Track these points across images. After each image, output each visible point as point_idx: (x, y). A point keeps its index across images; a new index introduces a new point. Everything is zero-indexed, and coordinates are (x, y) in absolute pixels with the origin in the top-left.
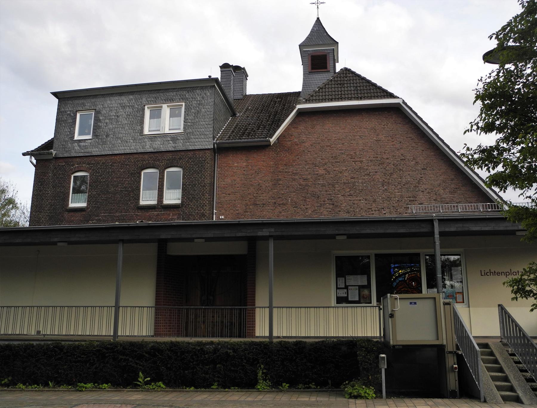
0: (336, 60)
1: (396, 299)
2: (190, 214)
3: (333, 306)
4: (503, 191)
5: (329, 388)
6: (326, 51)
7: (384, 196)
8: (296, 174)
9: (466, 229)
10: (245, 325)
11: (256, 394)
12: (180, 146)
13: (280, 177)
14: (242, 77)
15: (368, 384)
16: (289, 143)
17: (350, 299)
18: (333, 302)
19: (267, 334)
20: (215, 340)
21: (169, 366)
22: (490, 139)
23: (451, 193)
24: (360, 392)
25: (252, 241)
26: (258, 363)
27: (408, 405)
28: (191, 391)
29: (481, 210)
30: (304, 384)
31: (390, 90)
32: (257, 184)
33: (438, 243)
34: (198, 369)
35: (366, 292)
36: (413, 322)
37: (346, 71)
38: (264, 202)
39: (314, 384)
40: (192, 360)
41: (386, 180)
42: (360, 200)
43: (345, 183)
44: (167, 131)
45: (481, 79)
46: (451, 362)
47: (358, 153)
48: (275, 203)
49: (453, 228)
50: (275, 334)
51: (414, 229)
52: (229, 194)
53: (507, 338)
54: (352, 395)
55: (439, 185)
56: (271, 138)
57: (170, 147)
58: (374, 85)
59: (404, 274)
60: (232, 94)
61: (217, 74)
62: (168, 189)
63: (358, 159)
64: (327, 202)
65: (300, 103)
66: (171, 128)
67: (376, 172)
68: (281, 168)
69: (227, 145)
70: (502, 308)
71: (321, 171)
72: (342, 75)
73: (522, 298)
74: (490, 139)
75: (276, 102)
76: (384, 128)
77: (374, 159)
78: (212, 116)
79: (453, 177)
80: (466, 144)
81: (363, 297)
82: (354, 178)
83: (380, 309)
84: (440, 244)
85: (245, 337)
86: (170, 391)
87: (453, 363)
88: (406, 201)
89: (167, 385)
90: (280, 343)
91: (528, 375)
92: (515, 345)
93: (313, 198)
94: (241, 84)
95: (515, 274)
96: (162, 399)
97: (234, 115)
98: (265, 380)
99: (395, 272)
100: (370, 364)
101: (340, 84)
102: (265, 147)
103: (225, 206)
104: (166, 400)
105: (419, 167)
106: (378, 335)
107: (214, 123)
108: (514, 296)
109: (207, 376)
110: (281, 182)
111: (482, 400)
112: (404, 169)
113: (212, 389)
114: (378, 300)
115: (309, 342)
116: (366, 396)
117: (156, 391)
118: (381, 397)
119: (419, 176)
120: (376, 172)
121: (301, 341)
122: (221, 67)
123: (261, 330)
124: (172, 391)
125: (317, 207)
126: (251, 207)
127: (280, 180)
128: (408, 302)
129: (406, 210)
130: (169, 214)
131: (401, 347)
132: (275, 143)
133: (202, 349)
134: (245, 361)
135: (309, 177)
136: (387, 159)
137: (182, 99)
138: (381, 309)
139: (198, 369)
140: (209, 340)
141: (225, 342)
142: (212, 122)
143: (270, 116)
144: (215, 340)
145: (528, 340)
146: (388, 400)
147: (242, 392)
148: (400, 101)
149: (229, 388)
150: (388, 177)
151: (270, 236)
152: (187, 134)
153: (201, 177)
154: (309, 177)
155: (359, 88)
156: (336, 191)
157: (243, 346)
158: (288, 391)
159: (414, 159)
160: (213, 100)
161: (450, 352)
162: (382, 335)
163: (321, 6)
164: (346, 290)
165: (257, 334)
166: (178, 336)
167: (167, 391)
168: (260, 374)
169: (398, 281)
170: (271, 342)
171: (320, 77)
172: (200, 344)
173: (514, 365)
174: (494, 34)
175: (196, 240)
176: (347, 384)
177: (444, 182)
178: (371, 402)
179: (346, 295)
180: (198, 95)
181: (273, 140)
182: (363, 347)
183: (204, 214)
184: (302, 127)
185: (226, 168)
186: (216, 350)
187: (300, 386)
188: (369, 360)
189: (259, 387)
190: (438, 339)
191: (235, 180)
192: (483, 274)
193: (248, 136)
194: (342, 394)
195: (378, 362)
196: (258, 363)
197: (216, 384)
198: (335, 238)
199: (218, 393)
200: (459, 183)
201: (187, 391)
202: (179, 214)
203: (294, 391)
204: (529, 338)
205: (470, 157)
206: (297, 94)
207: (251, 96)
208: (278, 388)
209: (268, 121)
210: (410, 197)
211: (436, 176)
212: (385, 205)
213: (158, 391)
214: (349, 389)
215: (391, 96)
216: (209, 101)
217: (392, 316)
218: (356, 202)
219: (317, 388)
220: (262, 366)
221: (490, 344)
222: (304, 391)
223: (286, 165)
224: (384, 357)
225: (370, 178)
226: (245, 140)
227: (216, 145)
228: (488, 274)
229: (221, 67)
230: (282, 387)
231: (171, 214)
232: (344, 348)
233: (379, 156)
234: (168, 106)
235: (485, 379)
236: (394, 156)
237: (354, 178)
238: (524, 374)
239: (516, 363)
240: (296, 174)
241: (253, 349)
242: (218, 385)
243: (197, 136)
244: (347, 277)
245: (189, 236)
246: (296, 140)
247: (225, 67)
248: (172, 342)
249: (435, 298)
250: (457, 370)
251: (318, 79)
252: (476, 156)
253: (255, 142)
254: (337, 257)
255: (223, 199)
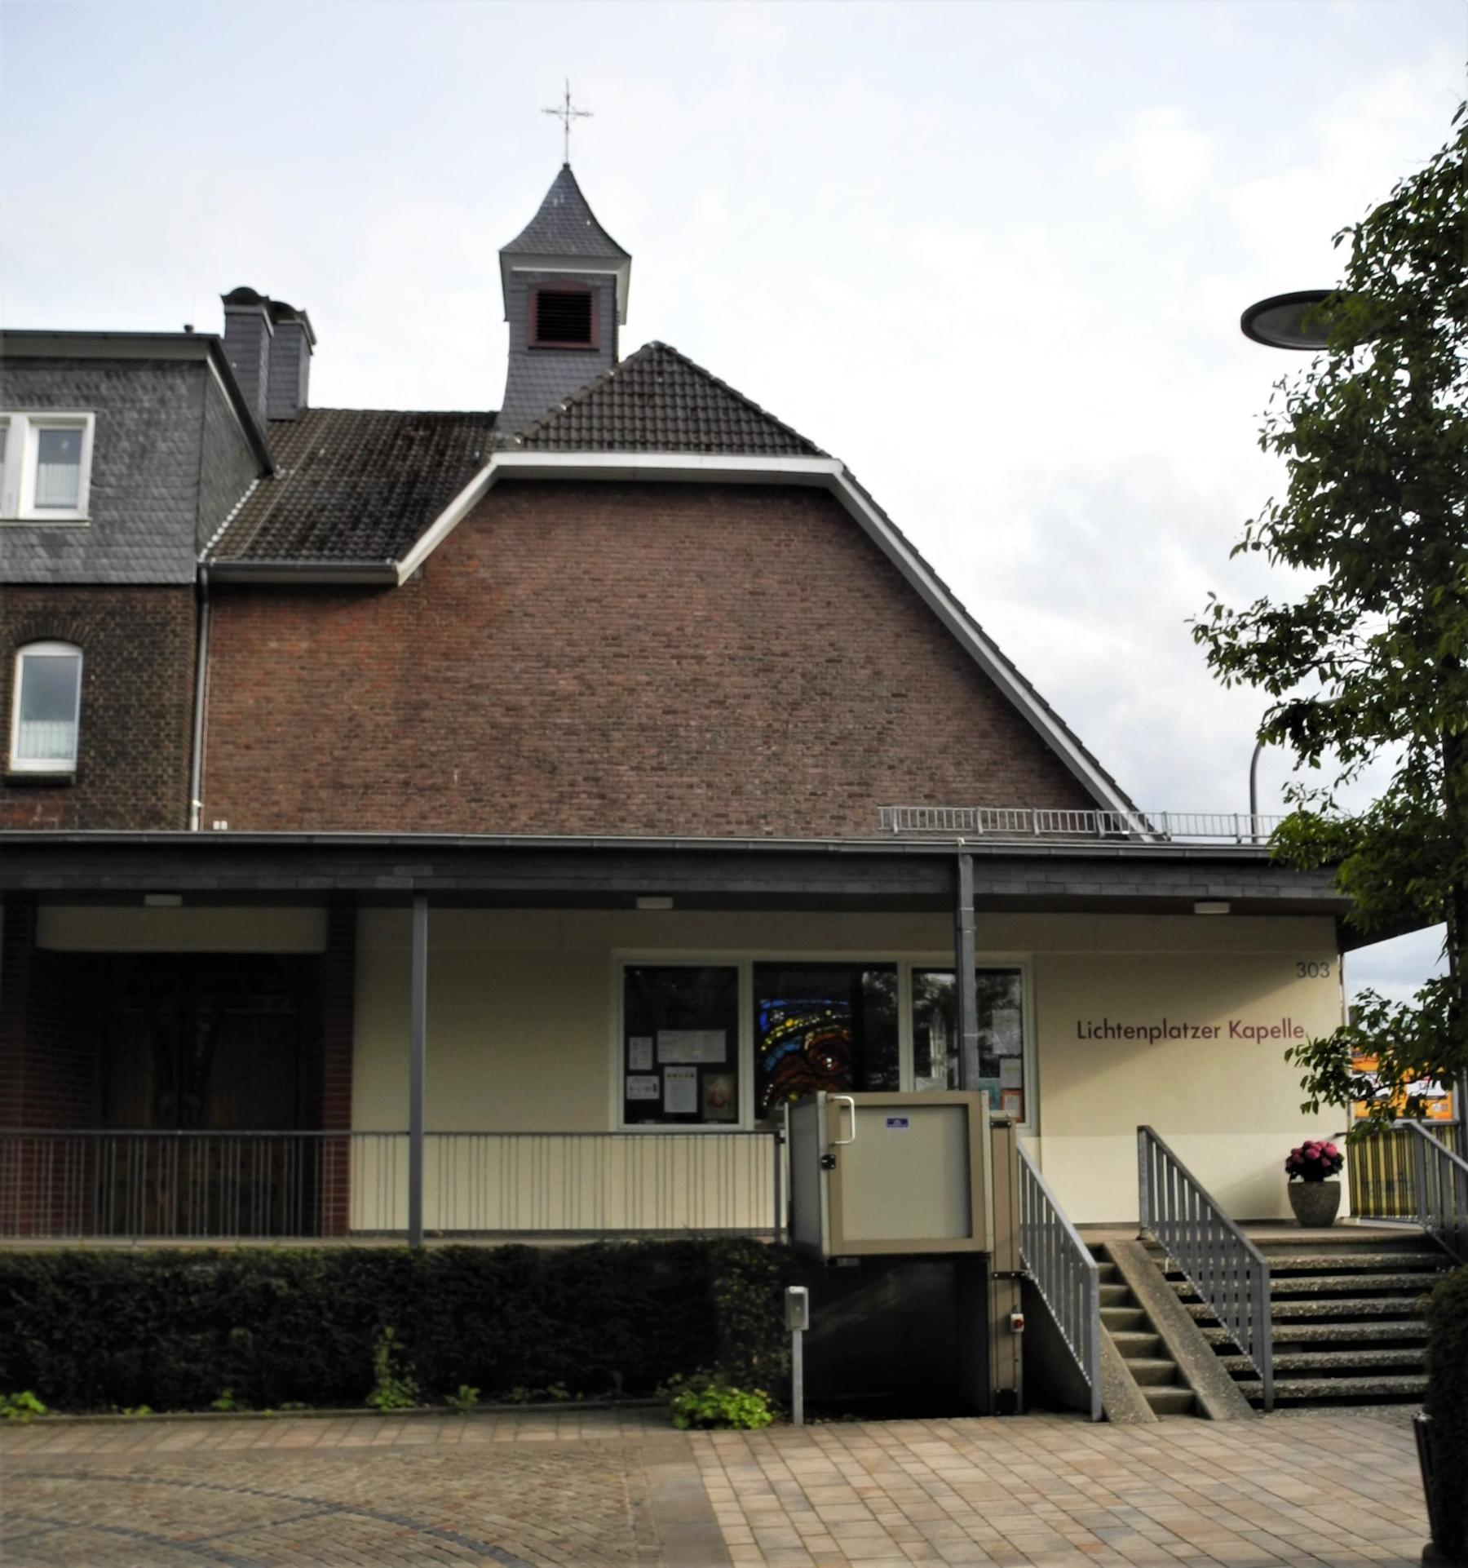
0: (621, 315)
1: (845, 1107)
2: (108, 813)
3: (612, 1128)
4: (1306, 762)
5: (614, 1398)
6: (590, 282)
7: (767, 776)
8: (479, 689)
9: (1055, 890)
10: (314, 1195)
11: (374, 1422)
12: (74, 567)
13: (424, 696)
14: (293, 345)
15: (747, 1381)
16: (460, 583)
17: (669, 1108)
18: (614, 1115)
19: (403, 1223)
20: (227, 1244)
21: (57, 1335)
22: (1293, 585)
23: (979, 776)
24: (724, 1406)
25: (343, 910)
26: (375, 1320)
27: (880, 1441)
28: (142, 1420)
29: (1102, 831)
30: (531, 1386)
31: (803, 430)
32: (347, 715)
33: (968, 931)
34: (165, 1345)
35: (721, 1085)
36: (888, 1183)
37: (660, 356)
38: (369, 778)
39: (561, 1384)
40: (141, 1315)
41: (777, 725)
42: (691, 786)
43: (643, 728)
44: (26, 510)
45: (1283, 382)
46: (1005, 1305)
47: (689, 630)
48: (406, 784)
49: (1016, 885)
50: (429, 1222)
51: (896, 885)
52: (248, 747)
53: (1161, 1226)
54: (698, 1417)
55: (943, 750)
56: (401, 559)
57: (39, 567)
58: (751, 408)
59: (802, 1031)
60: (262, 402)
61: (212, 321)
62: (27, 717)
63: (691, 651)
64: (583, 786)
65: (501, 446)
66: (42, 500)
67: (747, 697)
68: (431, 664)
69: (243, 577)
70: (1147, 1136)
71: (566, 684)
72: (646, 366)
73: (1332, 1104)
74: (1293, 585)
75: (411, 440)
76: (777, 554)
77: (741, 653)
78: (194, 469)
79: (987, 725)
80: (1212, 595)
81: (712, 1102)
82: (675, 712)
83: (779, 1141)
84: (977, 934)
85: (319, 1234)
86: (63, 1422)
87: (1010, 1308)
88: (837, 795)
89: (53, 1400)
90: (450, 1253)
91: (1221, 1333)
92: (1184, 1249)
93: (535, 772)
94: (293, 369)
95: (1175, 1033)
96: (41, 1451)
97: (266, 472)
98: (399, 1376)
99: (773, 1026)
100: (758, 1318)
101: (641, 395)
102: (386, 586)
103: (233, 788)
104: (57, 1456)
105: (884, 689)
106: (771, 1224)
107: (198, 493)
108: (1307, 1097)
109: (197, 1368)
110: (427, 714)
111: (1096, 1414)
112: (836, 692)
113: (215, 1409)
114: (760, 1113)
115: (547, 1251)
116: (741, 1421)
117: (12, 1424)
118: (788, 1418)
119: (882, 718)
120: (747, 697)
121: (520, 1248)
122: (228, 300)
123: (375, 1206)
124: (72, 1423)
125: (550, 802)
126: (323, 794)
127: (426, 705)
128: (882, 1119)
129: (838, 825)
130: (31, 810)
131: (855, 1262)
132: (412, 578)
133: (177, 1276)
134: (330, 1316)
135: (525, 700)
136: (785, 654)
137: (87, 399)
138: (782, 1141)
139: (165, 1345)
140: (203, 1244)
141: (259, 1253)
142: (190, 492)
143: (392, 488)
144: (227, 1244)
145: (1229, 1231)
146: (809, 1428)
147: (320, 1417)
148: (837, 472)
149: (275, 1407)
150: (785, 716)
151: (419, 893)
152: (102, 527)
153: (149, 684)
154: (525, 700)
155: (701, 415)
156: (613, 753)
157: (322, 1264)
158: (479, 1412)
159: (869, 660)
160: (197, 412)
161: (1004, 1276)
162: (784, 1224)
163: (577, 124)
164: (655, 1080)
165: (355, 1224)
166: (88, 1232)
167: (52, 1423)
168: (382, 1358)
169: (779, 1054)
170: (419, 1252)
171: (564, 366)
172: (169, 1259)
173: (1182, 1307)
174: (1347, 230)
175: (150, 900)
176: (677, 1383)
177: (959, 740)
178: (761, 1439)
179: (655, 1096)
180: (144, 388)
181: (407, 567)
182: (735, 1264)
183: (159, 813)
184: (506, 531)
185: (238, 657)
186: (226, 1281)
187: (518, 1392)
188: (753, 1303)
189: (379, 1400)
190: (969, 1235)
191: (268, 700)
192: (1085, 1032)
193: (321, 549)
194: (664, 1416)
195: (782, 1312)
196: (375, 1320)
197: (227, 1393)
198: (632, 906)
199: (238, 1424)
200: (1003, 747)
201: (125, 1422)
202: (69, 810)
203: (497, 1412)
204: (1233, 1226)
205: (1223, 640)
206: (486, 421)
207: (323, 412)
208: (444, 1403)
209: (386, 501)
210: (850, 784)
211: (935, 721)
212: (771, 805)
213: (20, 1424)
214: (685, 1400)
215: (806, 448)
216: (194, 415)
217: (829, 1163)
218: (677, 792)
219: (573, 1398)
220: (389, 1331)
221: (1110, 1246)
222: (532, 1411)
223: (446, 656)
224: (800, 1297)
225: (726, 713)
226: (308, 563)
227: (204, 575)
228: (1100, 1033)
229: (228, 300)
230: (459, 1398)
231: (39, 809)
232: (660, 1268)
233: (760, 646)
234: (32, 422)
235: (1106, 1359)
236: (805, 647)
237: (675, 712)
238: (1207, 1330)
239: (1185, 1299)
240: (479, 689)
241: (358, 1274)
242: (236, 1397)
243: (138, 537)
244: (663, 1037)
245: (129, 884)
246: (484, 573)
247: (240, 300)
248: (67, 1256)
249: (964, 1107)
250: (1021, 1330)
251: (557, 373)
252: (1245, 638)
253: (345, 569)
254: (629, 970)
255: (227, 763)
